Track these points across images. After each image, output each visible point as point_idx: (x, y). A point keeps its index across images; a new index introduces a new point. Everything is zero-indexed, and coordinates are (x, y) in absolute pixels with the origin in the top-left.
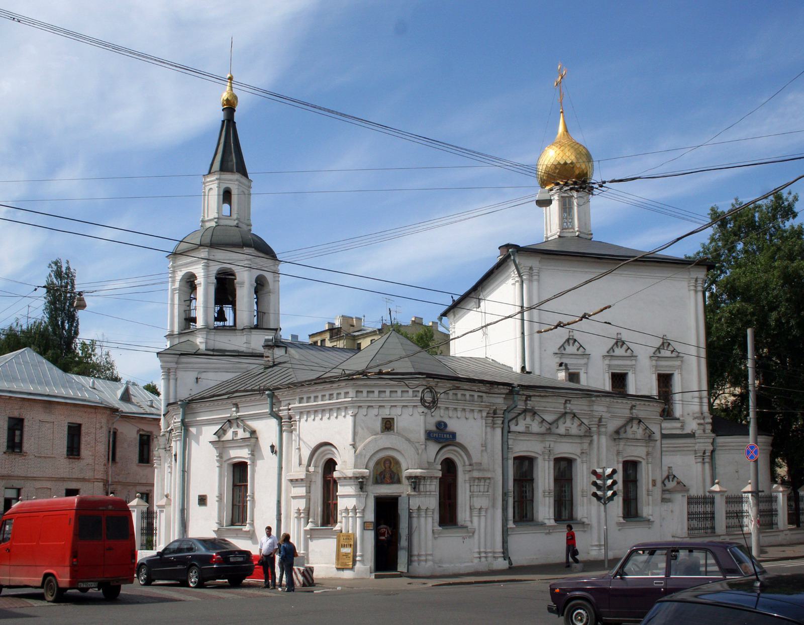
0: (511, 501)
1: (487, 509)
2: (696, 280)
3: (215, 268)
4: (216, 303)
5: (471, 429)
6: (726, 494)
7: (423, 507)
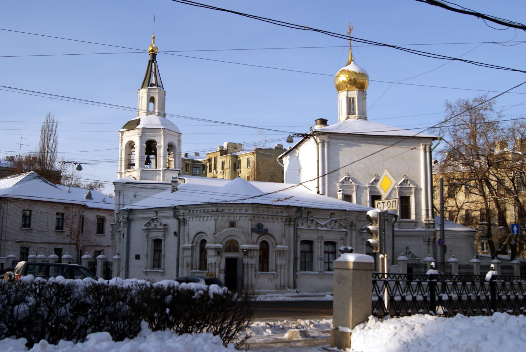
0: (299, 262)
1: (284, 265)
4: (146, 154)
5: (275, 227)
6: (501, 265)
7: (249, 263)
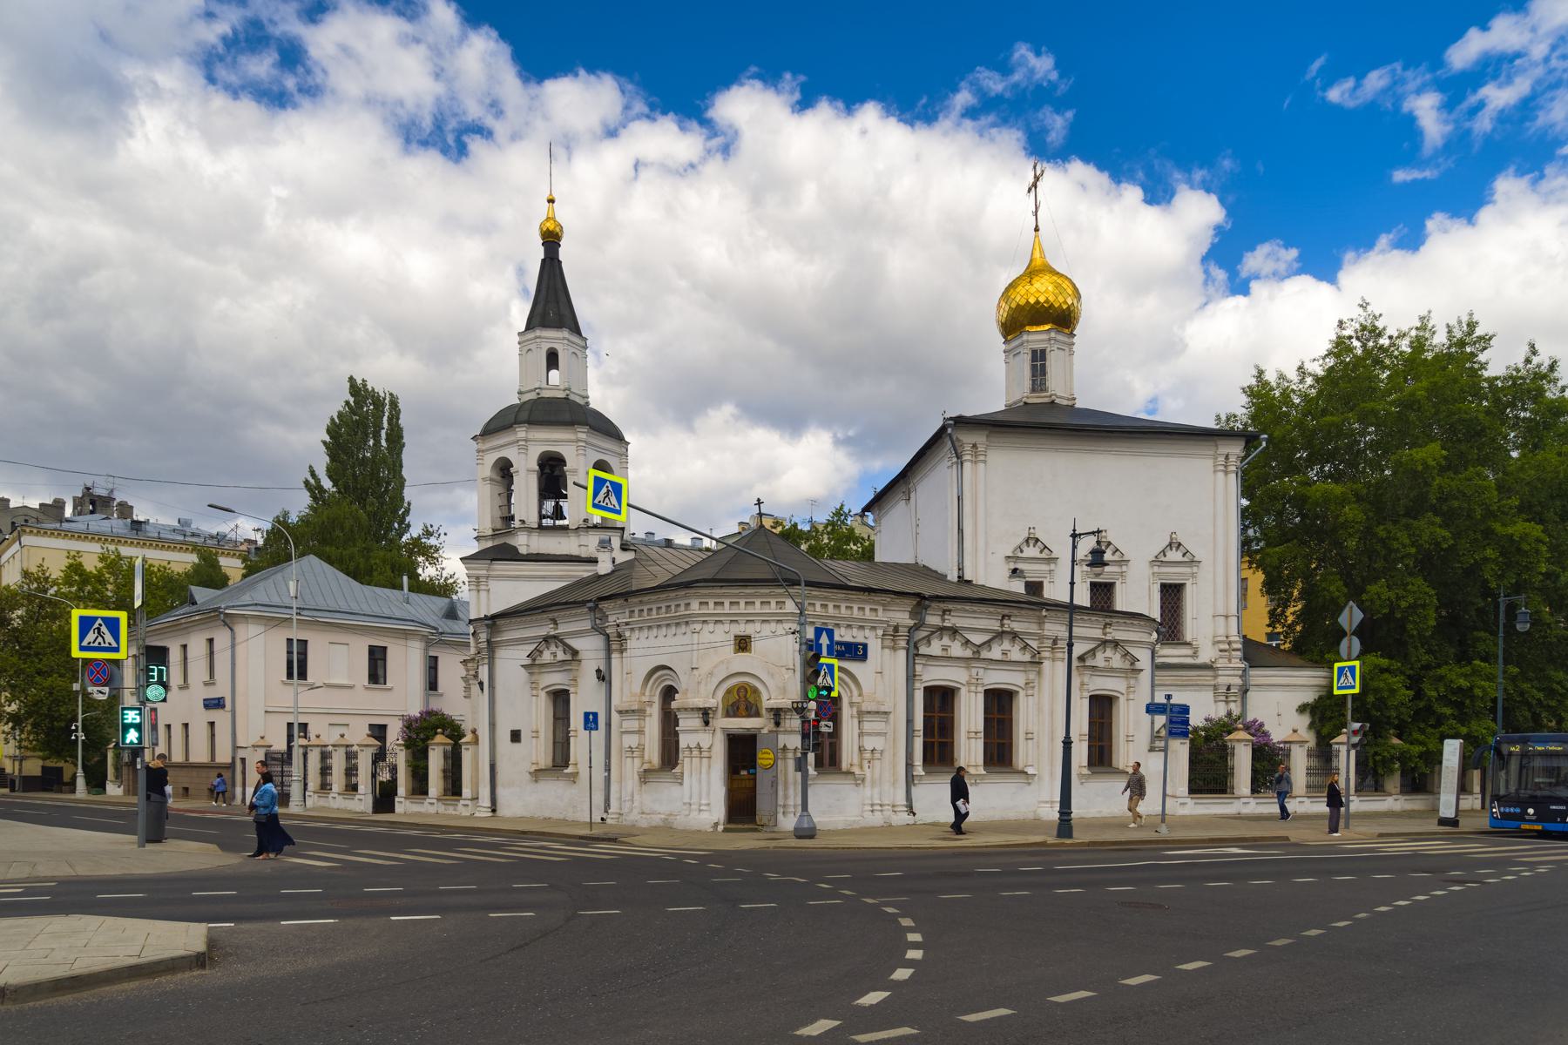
2: (1227, 457)
3: (535, 452)
